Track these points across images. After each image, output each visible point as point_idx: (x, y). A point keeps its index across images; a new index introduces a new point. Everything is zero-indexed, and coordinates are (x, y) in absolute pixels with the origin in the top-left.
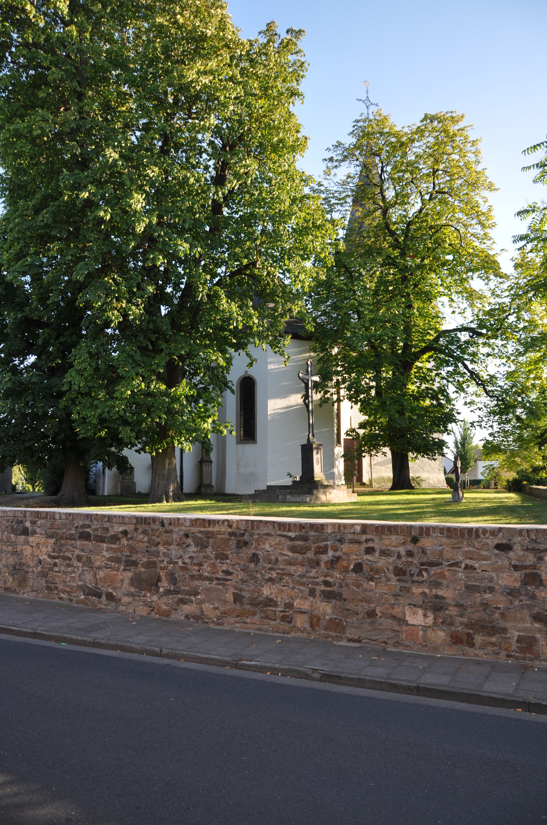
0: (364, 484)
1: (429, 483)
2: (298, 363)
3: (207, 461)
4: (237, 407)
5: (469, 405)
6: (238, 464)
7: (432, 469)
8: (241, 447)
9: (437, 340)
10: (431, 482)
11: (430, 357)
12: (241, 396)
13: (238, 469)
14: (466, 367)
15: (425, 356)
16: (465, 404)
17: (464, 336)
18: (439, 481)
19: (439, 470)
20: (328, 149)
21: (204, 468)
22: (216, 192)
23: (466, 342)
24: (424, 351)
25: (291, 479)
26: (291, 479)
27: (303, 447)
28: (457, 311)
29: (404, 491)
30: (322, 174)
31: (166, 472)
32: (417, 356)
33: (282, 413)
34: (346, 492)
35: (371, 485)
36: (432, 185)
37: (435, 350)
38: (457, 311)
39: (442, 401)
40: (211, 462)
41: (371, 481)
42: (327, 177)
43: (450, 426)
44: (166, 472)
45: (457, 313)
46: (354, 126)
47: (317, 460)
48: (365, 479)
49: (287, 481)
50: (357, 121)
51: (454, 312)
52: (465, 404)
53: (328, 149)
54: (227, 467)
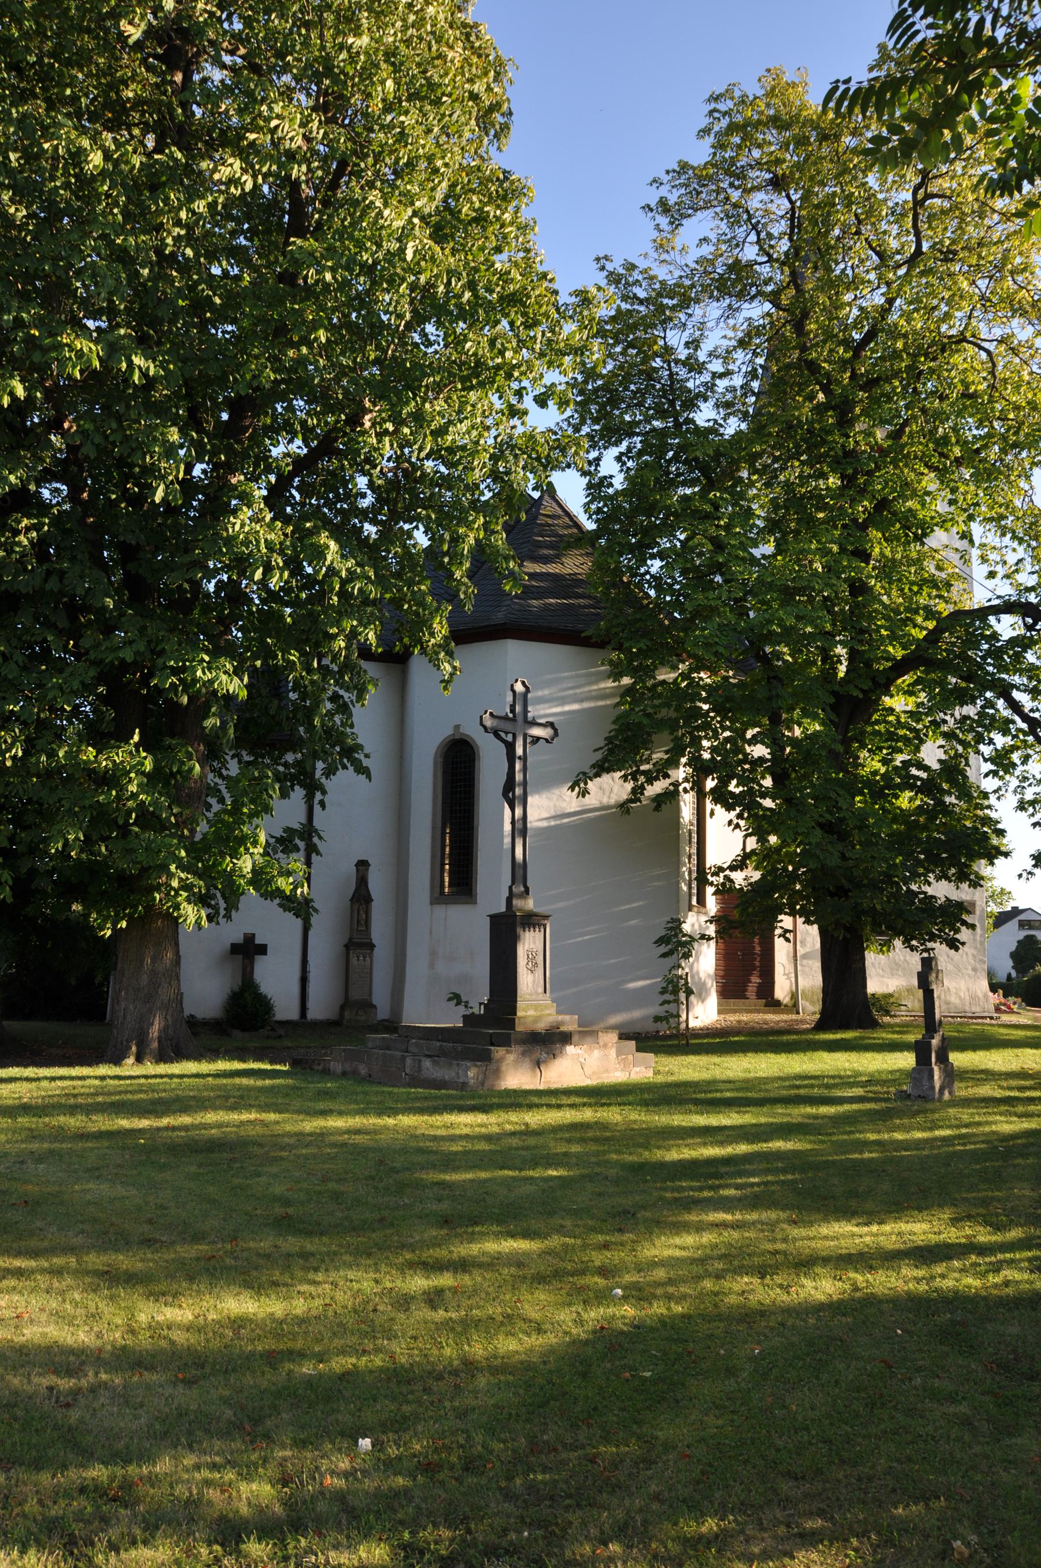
0: (777, 1004)
1: (948, 1003)
2: (586, 705)
3: (360, 945)
4: (434, 814)
5: (1031, 810)
6: (433, 954)
7: (957, 967)
8: (440, 910)
9: (933, 637)
10: (953, 999)
11: (917, 682)
12: (444, 787)
13: (432, 965)
14: (1015, 707)
15: (908, 679)
16: (1022, 806)
17: (1007, 627)
18: (974, 998)
19: (974, 970)
20: (656, 182)
21: (354, 960)
22: (759, 517)
23: (1013, 641)
24: (901, 667)
25: (462, 1010)
26: (462, 1010)
27: (494, 919)
28: (1001, 570)
29: (849, 1035)
30: (649, 248)
31: (145, 979)
32: (884, 684)
33: (549, 828)
34: (613, 1053)
35: (794, 1007)
36: (912, 237)
37: (931, 664)
38: (1001, 570)
39: (948, 799)
40: (372, 946)
41: (794, 996)
42: (664, 256)
43: (982, 867)
44: (145, 979)
45: (999, 576)
46: (711, 112)
47: (531, 958)
48: (782, 990)
49: (452, 1019)
50: (716, 98)
51: (992, 575)
52: (1022, 806)
53: (656, 182)
54: (408, 958)
